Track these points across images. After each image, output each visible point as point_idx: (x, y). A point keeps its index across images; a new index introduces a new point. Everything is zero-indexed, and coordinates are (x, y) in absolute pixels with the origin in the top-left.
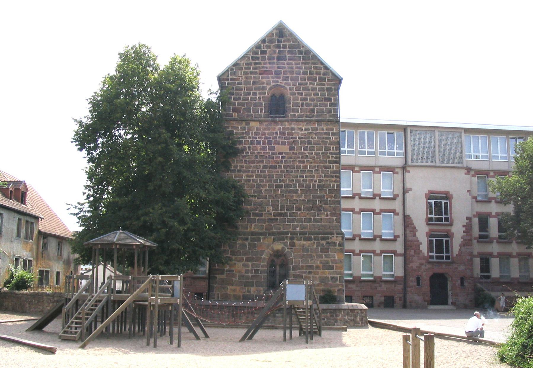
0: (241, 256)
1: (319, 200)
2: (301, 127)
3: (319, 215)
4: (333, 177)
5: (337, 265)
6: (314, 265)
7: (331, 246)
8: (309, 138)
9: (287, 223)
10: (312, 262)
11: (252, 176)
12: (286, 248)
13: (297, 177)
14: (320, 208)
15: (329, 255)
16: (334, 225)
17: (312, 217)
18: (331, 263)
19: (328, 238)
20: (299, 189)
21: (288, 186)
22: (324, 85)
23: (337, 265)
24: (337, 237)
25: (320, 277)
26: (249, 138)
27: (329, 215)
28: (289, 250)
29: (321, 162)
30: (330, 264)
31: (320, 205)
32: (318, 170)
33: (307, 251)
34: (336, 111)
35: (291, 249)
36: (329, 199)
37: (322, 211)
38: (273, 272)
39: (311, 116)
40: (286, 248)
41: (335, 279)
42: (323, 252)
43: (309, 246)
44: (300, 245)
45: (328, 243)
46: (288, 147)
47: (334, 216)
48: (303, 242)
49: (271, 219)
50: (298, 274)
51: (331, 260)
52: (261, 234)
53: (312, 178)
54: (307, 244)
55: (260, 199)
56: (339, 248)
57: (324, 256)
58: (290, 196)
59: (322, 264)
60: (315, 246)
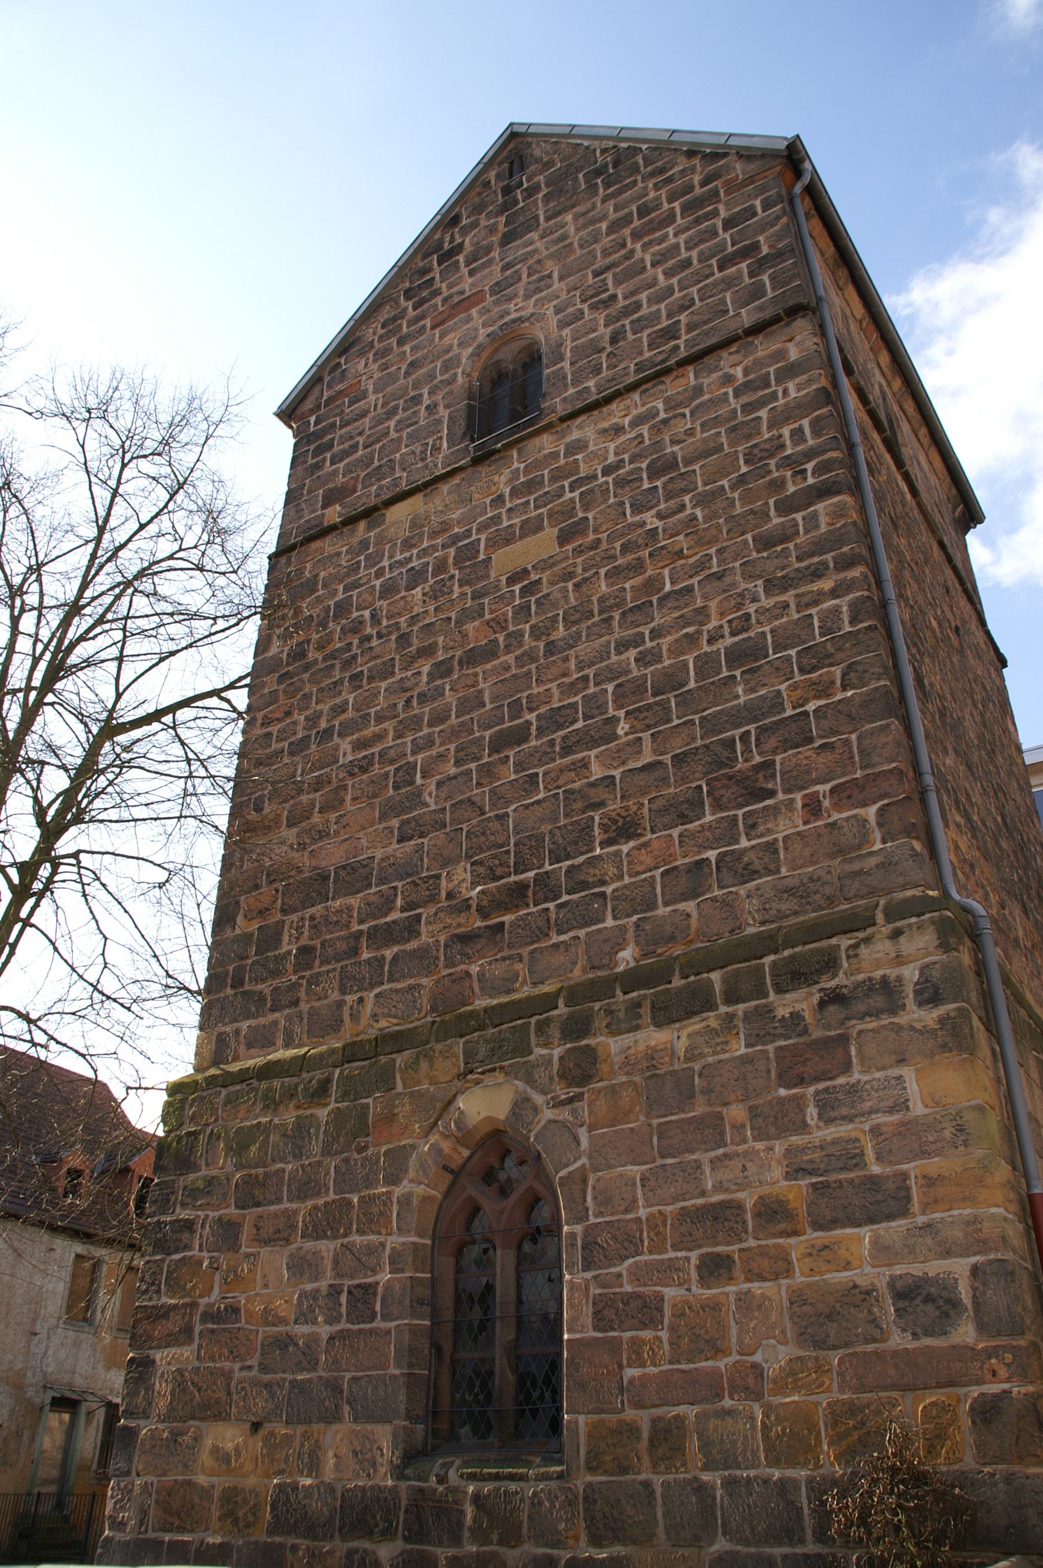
0: (286, 1205)
1: (745, 737)
2: (616, 420)
3: (754, 826)
4: (817, 574)
5: (934, 1165)
6: (741, 1195)
7: (861, 1018)
8: (658, 445)
9: (556, 939)
10: (725, 1175)
11: (380, 737)
12: (539, 1099)
13: (604, 655)
14: (761, 783)
15: (853, 1089)
16: (872, 861)
17: (712, 855)
18: (879, 1159)
19: (829, 963)
20: (621, 713)
21: (555, 720)
22: (715, 213)
23: (934, 1165)
24: (897, 934)
25: (797, 1298)
26: (380, 573)
27: (826, 803)
28: (564, 1114)
29: (737, 526)
30: (876, 1169)
31: (758, 759)
32: (719, 576)
33: (688, 1096)
34: (748, 154)
35: (571, 1100)
36: (811, 707)
37: (772, 793)
38: (483, 1299)
39: (660, 358)
40: (539, 1099)
41: (929, 1299)
42: (801, 1081)
43: (691, 1055)
44: (629, 1064)
45: (834, 998)
46: (555, 531)
47: (865, 804)
48: (654, 1037)
49: (465, 939)
50: (628, 1288)
51: (876, 1131)
52: (396, 1041)
53: (690, 630)
54: (681, 1046)
55: (410, 839)
56: (929, 1016)
57: (812, 1112)
58: (573, 767)
59: (804, 1182)
60: (740, 1048)
